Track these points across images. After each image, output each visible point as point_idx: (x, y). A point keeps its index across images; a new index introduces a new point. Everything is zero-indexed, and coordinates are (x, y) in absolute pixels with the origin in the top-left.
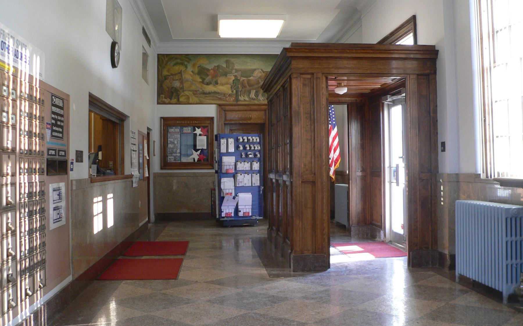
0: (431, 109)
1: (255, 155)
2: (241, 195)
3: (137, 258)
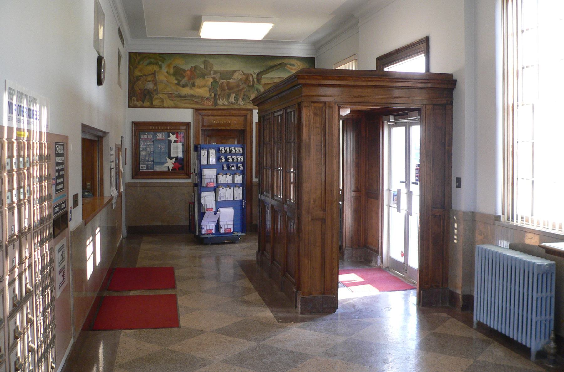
0: (446, 142)
1: (238, 167)
2: (222, 210)
3: (125, 294)
